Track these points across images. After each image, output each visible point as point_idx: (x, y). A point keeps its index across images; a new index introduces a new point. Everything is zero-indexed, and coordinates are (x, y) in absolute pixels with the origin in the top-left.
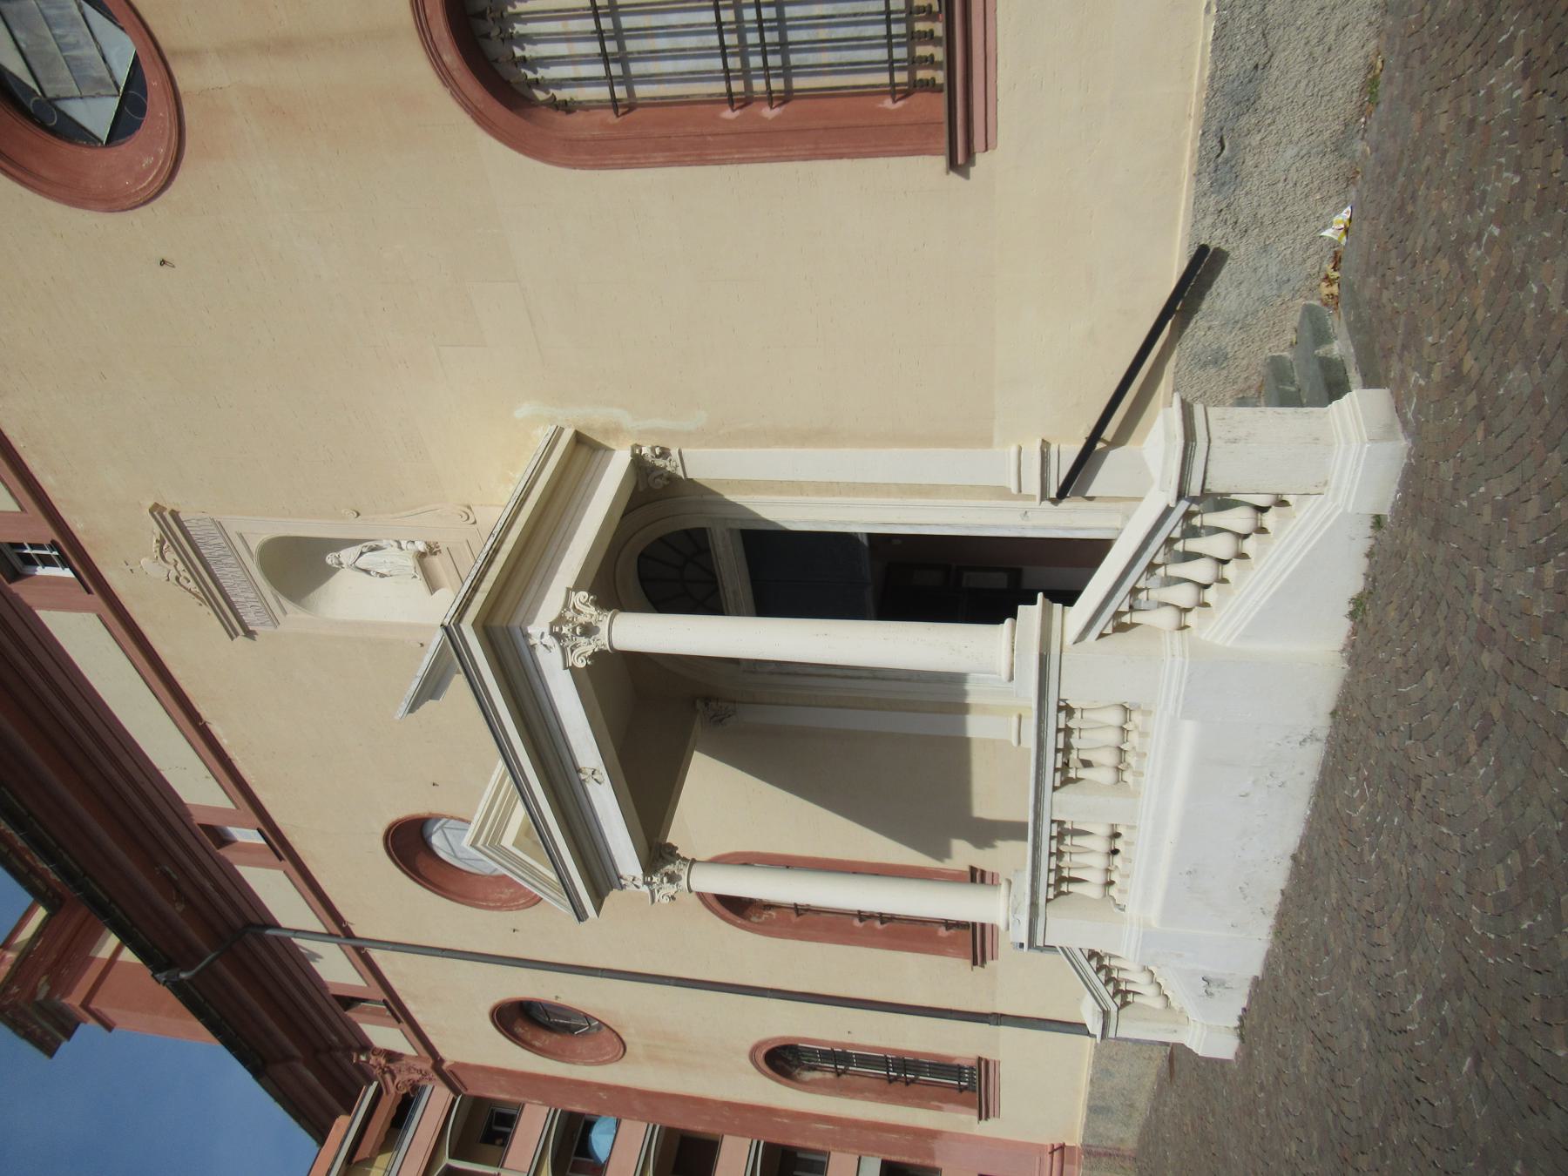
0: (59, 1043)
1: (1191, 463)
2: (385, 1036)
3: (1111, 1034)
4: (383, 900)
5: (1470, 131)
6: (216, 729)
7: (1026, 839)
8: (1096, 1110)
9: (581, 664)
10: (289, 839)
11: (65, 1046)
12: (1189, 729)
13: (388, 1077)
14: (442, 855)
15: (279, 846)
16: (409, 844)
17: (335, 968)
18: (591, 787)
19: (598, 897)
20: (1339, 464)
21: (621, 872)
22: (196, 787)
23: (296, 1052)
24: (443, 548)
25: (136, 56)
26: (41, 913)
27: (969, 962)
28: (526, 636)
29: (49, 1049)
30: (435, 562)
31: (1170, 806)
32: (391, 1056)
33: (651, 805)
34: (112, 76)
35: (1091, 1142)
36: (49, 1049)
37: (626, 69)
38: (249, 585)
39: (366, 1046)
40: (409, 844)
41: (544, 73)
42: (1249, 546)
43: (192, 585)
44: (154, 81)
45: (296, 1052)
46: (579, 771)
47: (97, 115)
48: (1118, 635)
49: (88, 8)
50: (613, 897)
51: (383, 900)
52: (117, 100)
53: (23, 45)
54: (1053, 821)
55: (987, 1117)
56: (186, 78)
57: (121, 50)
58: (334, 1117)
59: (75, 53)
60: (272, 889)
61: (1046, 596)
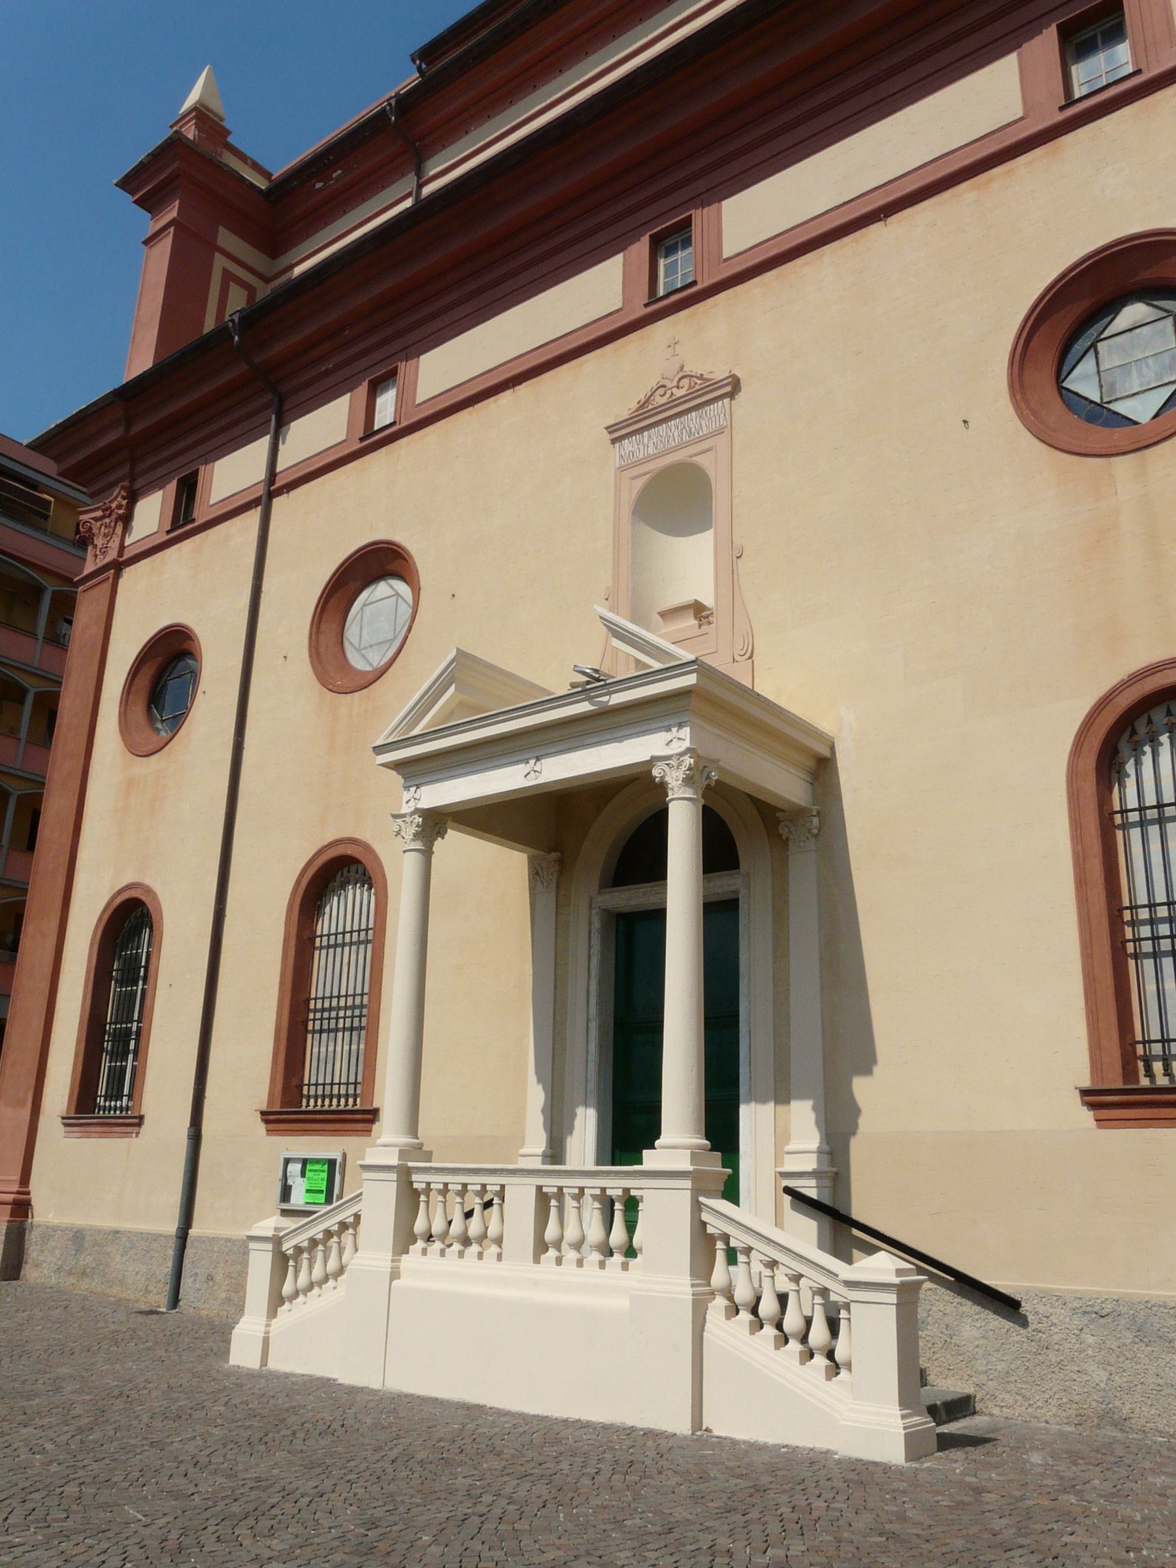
0: (132, 193)
1: (876, 1290)
2: (151, 513)
3: (252, 1245)
4: (316, 533)
5: (1160, 1495)
6: (506, 397)
7: (598, 1164)
8: (78, 1237)
9: (656, 772)
10: (384, 449)
11: (129, 198)
12: (624, 1303)
13: (99, 513)
14: (364, 595)
15: (372, 440)
16: (380, 562)
17: (234, 472)
18: (522, 769)
19: (398, 766)
20: (858, 1417)
21: (423, 789)
22: (441, 368)
23: (136, 429)
24: (705, 628)
25: (1136, 423)
26: (262, 184)
27: (264, 1108)
28: (680, 726)
29: (128, 183)
30: (690, 622)
31: (501, 1297)
32: (127, 520)
33: (489, 819)
34: (1116, 400)
35: (88, 1238)
36: (128, 183)
37: (1152, 822)
38: (657, 446)
39: (133, 498)
40: (380, 562)
41: (1147, 760)
42: (794, 1346)
43: (659, 400)
44: (1118, 435)
45: (136, 429)
46: (538, 759)
47: (1083, 381)
48: (504, 1245)
49: (1169, 390)
50: (395, 779)
51: (316, 533)
52: (1099, 401)
53: (1138, 331)
54: (503, 1186)
55: (66, 1125)
56: (1123, 466)
57: (1141, 409)
58: (57, 459)
59: (1134, 372)
60: (321, 427)
61: (729, 1176)
